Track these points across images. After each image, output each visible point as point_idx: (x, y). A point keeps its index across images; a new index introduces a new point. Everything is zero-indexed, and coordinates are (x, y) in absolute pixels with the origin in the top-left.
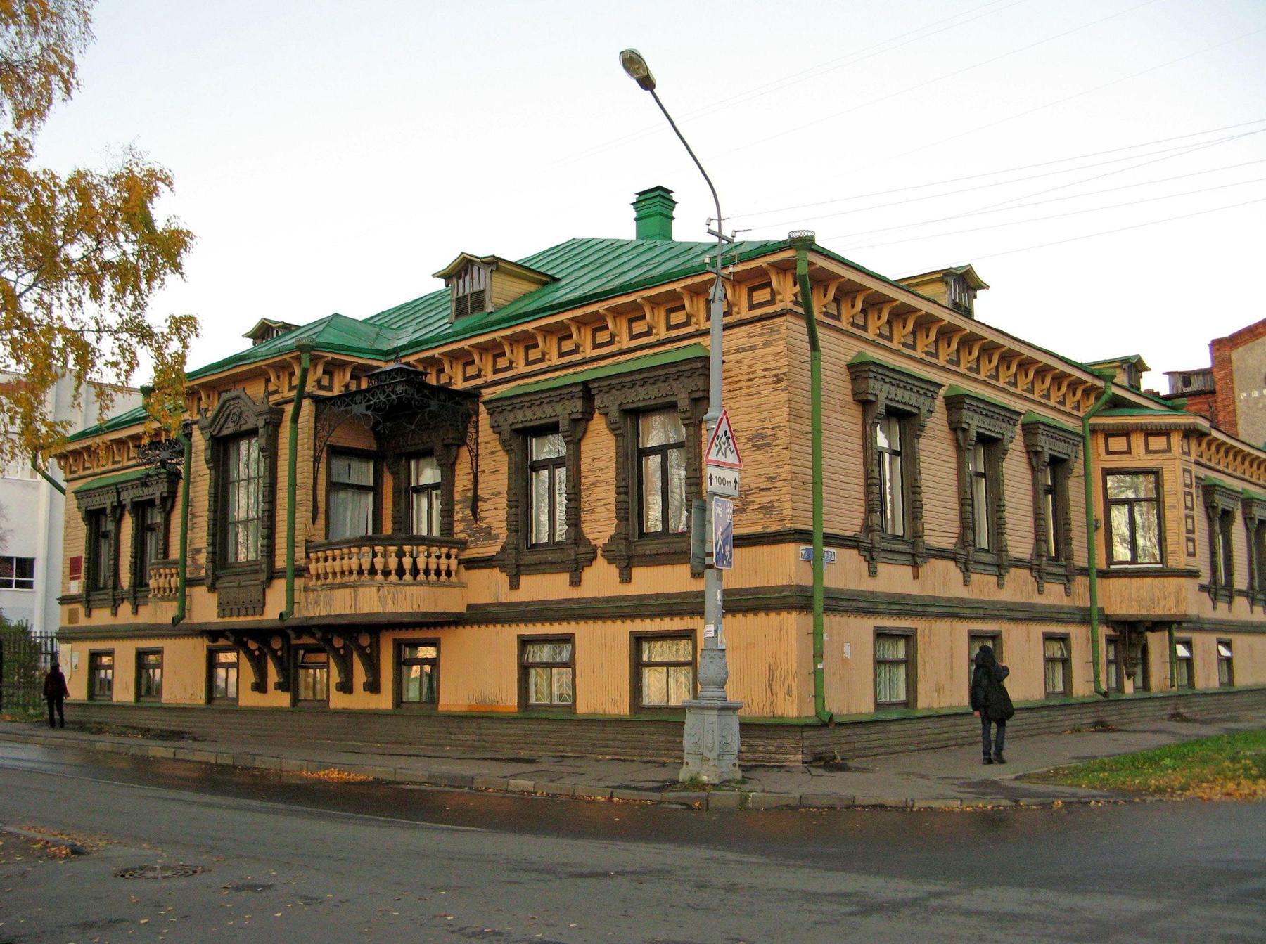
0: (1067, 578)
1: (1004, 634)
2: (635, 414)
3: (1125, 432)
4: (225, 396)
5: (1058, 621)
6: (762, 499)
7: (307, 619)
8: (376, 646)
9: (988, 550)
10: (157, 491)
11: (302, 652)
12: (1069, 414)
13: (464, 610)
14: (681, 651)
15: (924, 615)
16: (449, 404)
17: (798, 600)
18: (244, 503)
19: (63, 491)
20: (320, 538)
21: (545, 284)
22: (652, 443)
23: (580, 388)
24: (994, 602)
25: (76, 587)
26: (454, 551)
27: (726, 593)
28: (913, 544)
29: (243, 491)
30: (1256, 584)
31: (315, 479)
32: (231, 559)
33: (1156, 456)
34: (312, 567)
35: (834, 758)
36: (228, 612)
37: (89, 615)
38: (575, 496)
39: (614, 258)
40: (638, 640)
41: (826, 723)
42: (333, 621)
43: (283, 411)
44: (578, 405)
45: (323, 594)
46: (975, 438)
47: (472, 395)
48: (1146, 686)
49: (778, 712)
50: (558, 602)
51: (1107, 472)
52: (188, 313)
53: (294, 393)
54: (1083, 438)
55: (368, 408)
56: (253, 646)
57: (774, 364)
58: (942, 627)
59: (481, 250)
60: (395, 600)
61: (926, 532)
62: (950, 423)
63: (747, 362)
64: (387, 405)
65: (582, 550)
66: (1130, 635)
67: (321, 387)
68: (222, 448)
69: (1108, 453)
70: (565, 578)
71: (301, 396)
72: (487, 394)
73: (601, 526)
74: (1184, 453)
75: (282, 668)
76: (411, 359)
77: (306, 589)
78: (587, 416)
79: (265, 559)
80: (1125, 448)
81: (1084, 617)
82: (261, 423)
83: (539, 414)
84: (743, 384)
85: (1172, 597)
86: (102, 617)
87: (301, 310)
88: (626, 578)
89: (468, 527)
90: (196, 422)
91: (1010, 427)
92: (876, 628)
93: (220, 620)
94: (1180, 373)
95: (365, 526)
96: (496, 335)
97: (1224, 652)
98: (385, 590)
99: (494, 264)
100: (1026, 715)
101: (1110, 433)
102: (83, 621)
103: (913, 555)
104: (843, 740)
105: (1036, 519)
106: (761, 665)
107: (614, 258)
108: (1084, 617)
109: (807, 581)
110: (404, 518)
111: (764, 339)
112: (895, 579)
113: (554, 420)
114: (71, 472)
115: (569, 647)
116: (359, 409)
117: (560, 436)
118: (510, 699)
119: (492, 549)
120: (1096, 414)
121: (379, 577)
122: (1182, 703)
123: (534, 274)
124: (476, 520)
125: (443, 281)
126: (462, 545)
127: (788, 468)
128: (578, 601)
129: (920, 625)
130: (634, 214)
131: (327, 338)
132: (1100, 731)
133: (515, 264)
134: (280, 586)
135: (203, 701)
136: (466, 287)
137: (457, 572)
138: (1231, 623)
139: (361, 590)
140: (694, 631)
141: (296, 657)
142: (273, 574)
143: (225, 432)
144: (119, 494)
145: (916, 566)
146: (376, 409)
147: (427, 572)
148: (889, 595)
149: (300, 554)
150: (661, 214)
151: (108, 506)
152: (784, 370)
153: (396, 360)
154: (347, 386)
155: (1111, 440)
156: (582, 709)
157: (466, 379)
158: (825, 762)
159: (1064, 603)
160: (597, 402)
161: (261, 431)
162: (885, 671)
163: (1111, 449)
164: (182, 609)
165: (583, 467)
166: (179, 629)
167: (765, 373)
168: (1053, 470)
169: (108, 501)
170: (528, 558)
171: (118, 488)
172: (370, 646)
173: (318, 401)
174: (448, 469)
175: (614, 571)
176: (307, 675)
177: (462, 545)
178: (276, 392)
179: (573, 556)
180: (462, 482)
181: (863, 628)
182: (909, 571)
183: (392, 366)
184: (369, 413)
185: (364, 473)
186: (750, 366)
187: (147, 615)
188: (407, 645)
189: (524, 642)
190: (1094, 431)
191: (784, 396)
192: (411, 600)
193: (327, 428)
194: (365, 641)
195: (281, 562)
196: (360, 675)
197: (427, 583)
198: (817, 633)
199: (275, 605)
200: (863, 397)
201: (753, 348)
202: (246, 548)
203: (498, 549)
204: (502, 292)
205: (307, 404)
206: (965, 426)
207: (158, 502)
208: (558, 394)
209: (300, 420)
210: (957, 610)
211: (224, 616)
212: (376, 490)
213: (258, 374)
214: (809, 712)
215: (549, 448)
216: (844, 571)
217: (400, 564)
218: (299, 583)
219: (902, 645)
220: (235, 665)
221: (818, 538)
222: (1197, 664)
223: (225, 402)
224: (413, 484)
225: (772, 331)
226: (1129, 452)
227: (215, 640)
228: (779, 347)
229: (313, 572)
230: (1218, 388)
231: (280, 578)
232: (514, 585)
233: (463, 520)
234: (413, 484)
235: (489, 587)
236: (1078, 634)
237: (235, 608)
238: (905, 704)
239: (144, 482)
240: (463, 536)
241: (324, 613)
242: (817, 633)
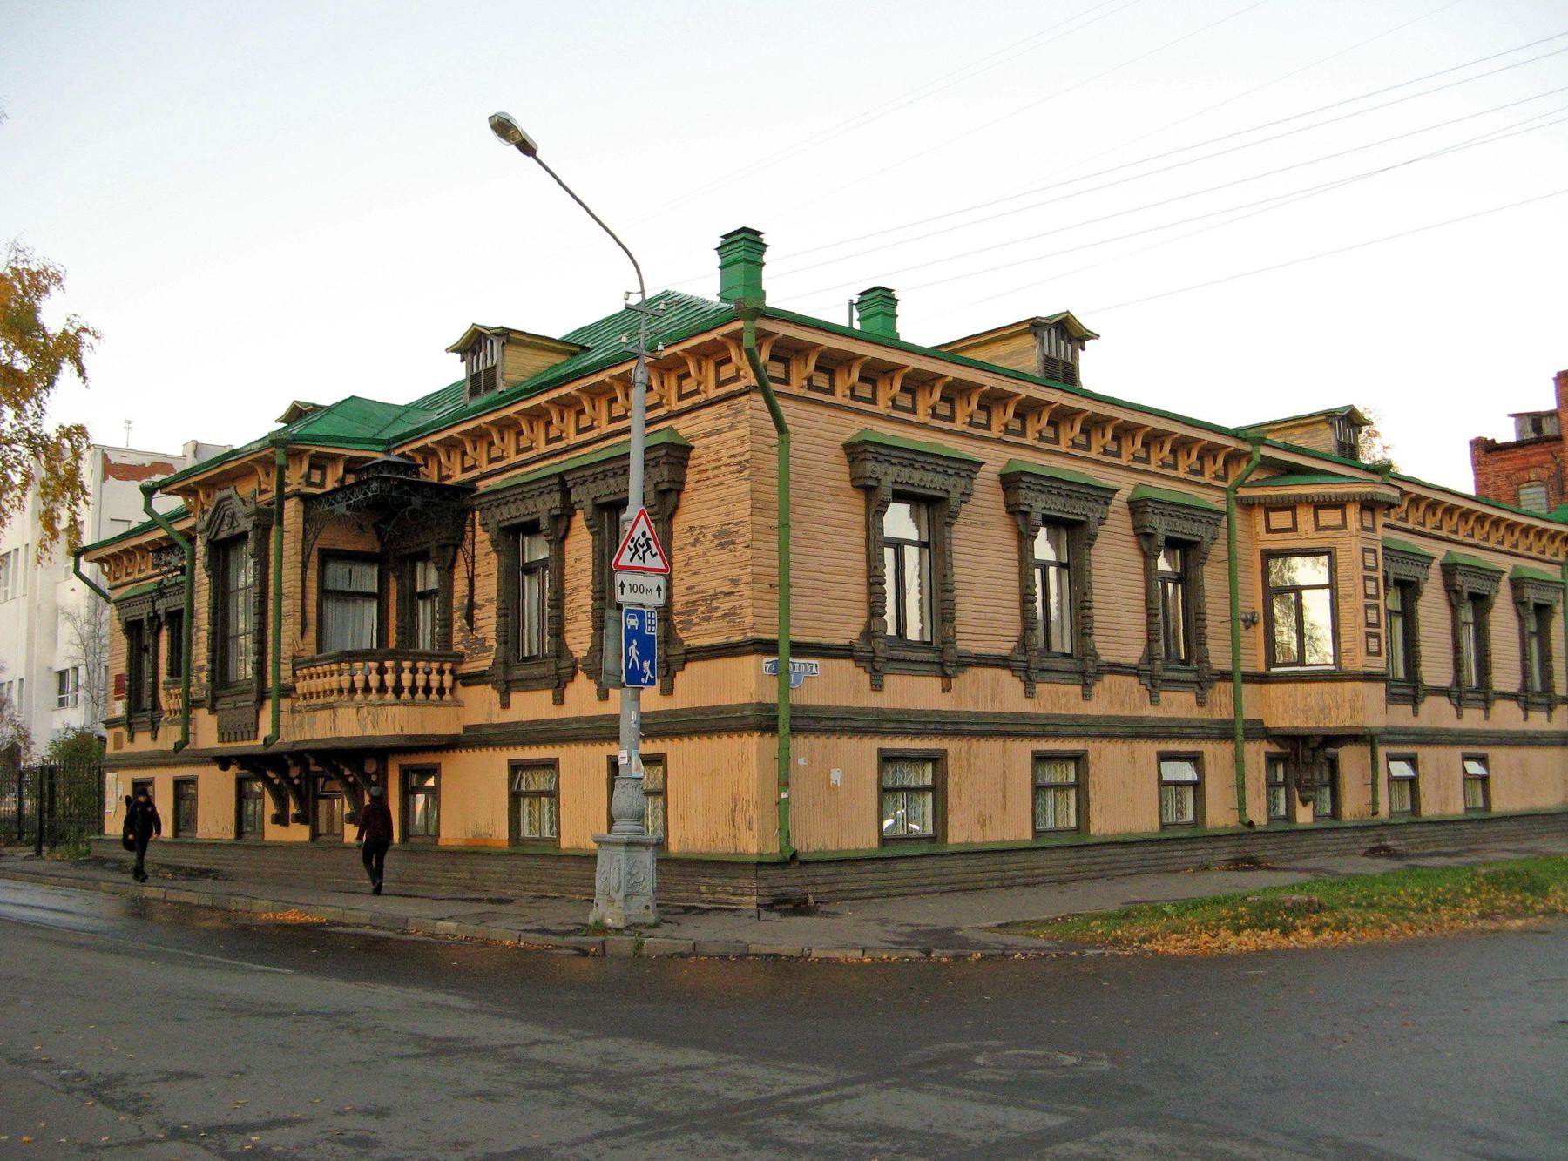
1: (1092, 756)
3: (1290, 505)
5: (1182, 737)
6: (725, 605)
7: (295, 743)
9: (1070, 655)
11: (321, 780)
12: (1209, 486)
13: (460, 731)
15: (955, 734)
17: (763, 721)
19: (107, 598)
20: (310, 650)
21: (574, 354)
23: (555, 481)
24: (1074, 717)
25: (119, 709)
26: (447, 666)
27: (643, 716)
28: (942, 651)
29: (241, 599)
32: (232, 678)
33: (1328, 533)
35: (806, 901)
37: (132, 740)
41: (792, 860)
42: (344, 745)
45: (307, 715)
47: (467, 488)
48: (1336, 813)
49: (741, 849)
50: (543, 722)
52: (79, 422)
54: (1227, 514)
55: (348, 507)
57: (739, 450)
58: (989, 749)
59: (492, 321)
60: (375, 722)
61: (959, 636)
62: (1008, 506)
63: (715, 448)
64: (377, 504)
65: (564, 663)
66: (1306, 756)
67: (309, 484)
68: (222, 552)
69: (1269, 530)
74: (1363, 528)
75: (301, 801)
76: (406, 449)
77: (293, 711)
80: (1289, 524)
81: (1224, 732)
82: (249, 526)
83: (523, 510)
84: (710, 474)
85: (1347, 705)
89: (465, 638)
91: (1100, 508)
92: (881, 751)
93: (220, 745)
94: (1529, 414)
95: (369, 641)
97: (1474, 768)
98: (364, 711)
99: (507, 336)
100: (1118, 851)
101: (1271, 506)
102: (128, 748)
103: (941, 664)
104: (819, 880)
105: (1148, 615)
106: (717, 798)
108: (1224, 732)
109: (771, 698)
110: (408, 631)
111: (729, 420)
112: (1058, 699)
114: (116, 579)
115: (660, 768)
116: (341, 509)
118: (502, 832)
119: (484, 663)
121: (359, 696)
122: (1397, 837)
124: (472, 630)
126: (459, 659)
127: (749, 569)
128: (560, 721)
129: (952, 746)
130: (718, 262)
132: (1245, 869)
135: (232, 837)
137: (452, 691)
138: (1488, 734)
139: (340, 711)
141: (316, 786)
143: (222, 535)
145: (945, 676)
147: (413, 690)
148: (901, 712)
149: (286, 671)
150: (746, 261)
151: (145, 617)
152: (747, 456)
153: (387, 452)
154: (342, 480)
155: (1321, 513)
158: (791, 905)
159: (1195, 715)
162: (889, 799)
163: (1273, 526)
164: (186, 733)
165: (567, 570)
167: (732, 460)
170: (517, 673)
172: (376, 772)
173: (306, 499)
174: (447, 572)
177: (459, 659)
180: (460, 587)
182: (936, 683)
183: (381, 457)
185: (368, 579)
186: (717, 452)
188: (415, 772)
190: (1248, 505)
191: (747, 486)
192: (394, 722)
194: (371, 767)
197: (412, 702)
198: (784, 759)
200: (862, 482)
201: (719, 431)
202: (244, 669)
203: (490, 662)
204: (516, 368)
206: (1024, 508)
210: (1010, 728)
212: (381, 597)
214: (773, 848)
215: (536, 550)
217: (382, 682)
218: (285, 704)
219: (929, 768)
221: (784, 648)
222: (1424, 786)
223: (219, 502)
224: (419, 589)
225: (738, 412)
226: (1294, 529)
228: (743, 430)
230: (1565, 432)
233: (461, 630)
234: (419, 589)
235: (481, 706)
236: (1216, 753)
238: (932, 839)
240: (459, 648)
241: (308, 737)
242: (784, 759)
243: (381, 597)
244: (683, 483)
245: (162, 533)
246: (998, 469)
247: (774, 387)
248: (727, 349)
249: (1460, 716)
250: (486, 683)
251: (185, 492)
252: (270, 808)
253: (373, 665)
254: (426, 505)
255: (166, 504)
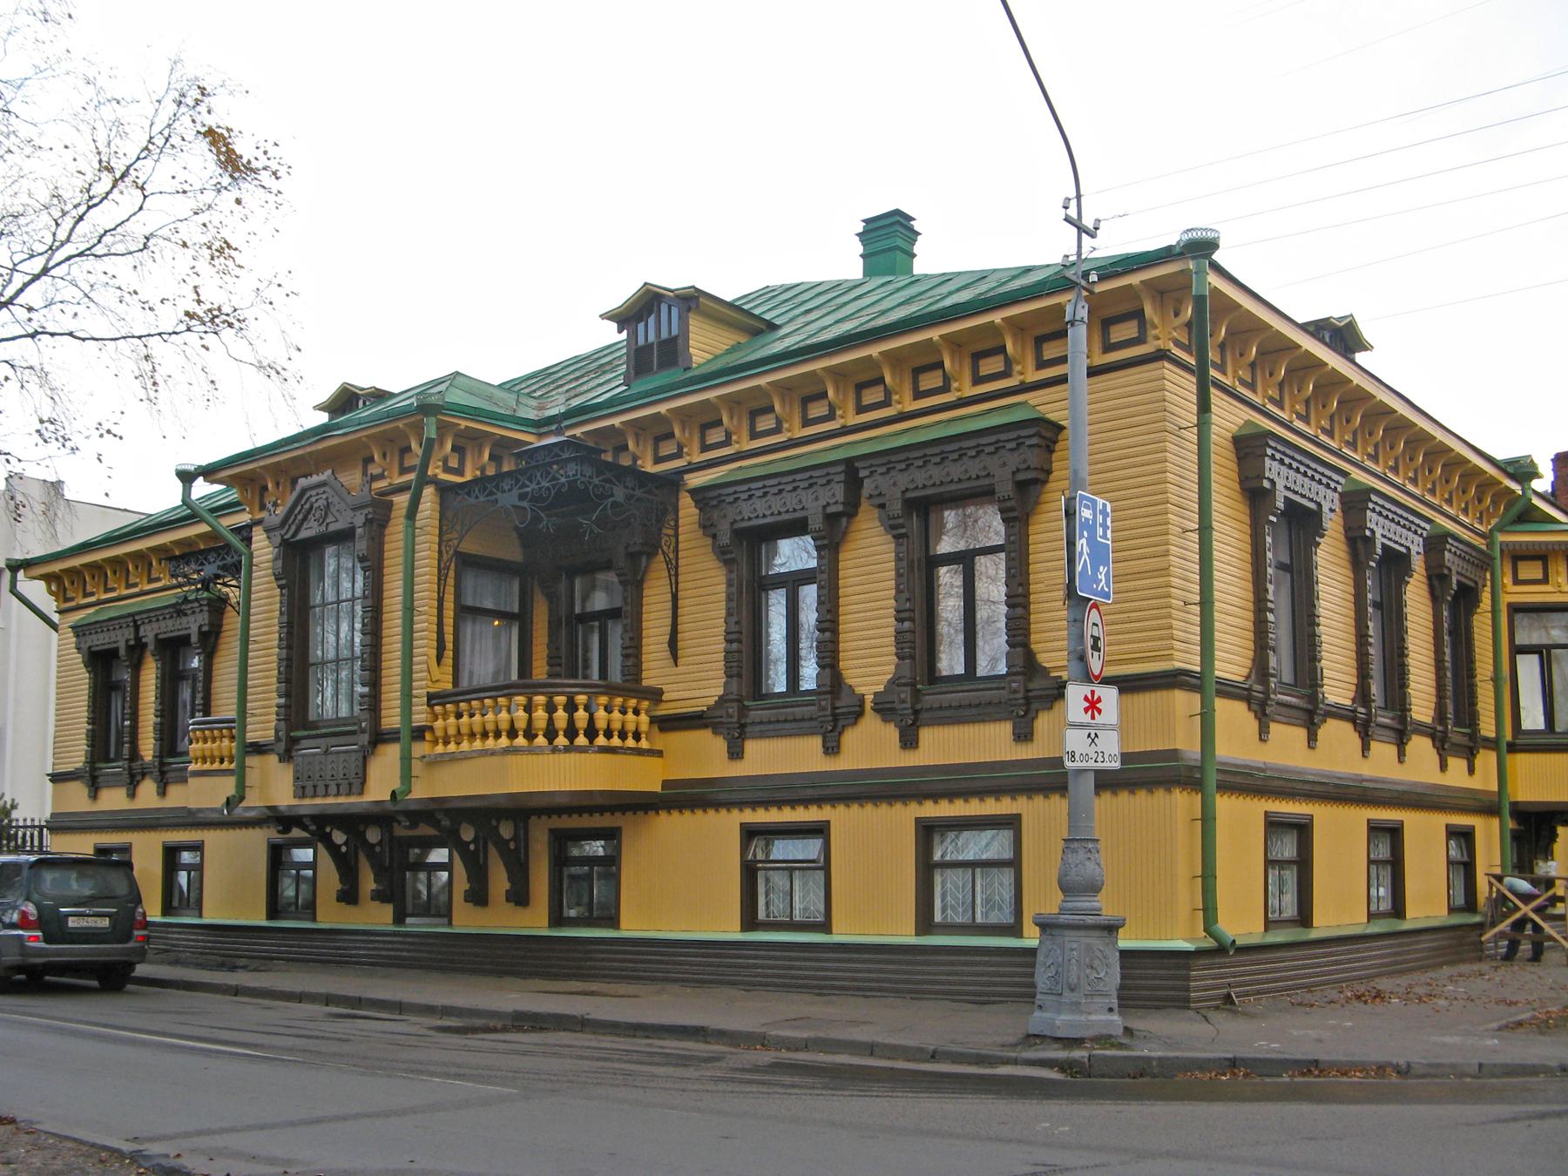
0: (1469, 754)
2: (921, 511)
4: (303, 482)
8: (522, 837)
10: (194, 624)
13: (659, 789)
14: (809, 849)
16: (638, 493)
18: (338, 635)
19: (54, 626)
22: (945, 546)
23: (840, 468)
30: (1375, 689)
31: (441, 601)
32: (312, 716)
34: (439, 724)
36: (309, 790)
38: (829, 623)
39: (856, 299)
40: (928, 831)
43: (390, 505)
44: (838, 491)
46: (1280, 505)
47: (672, 482)
51: (1515, 609)
53: (412, 476)
55: (522, 497)
56: (339, 837)
59: (672, 279)
67: (447, 470)
68: (298, 560)
69: (1516, 582)
70: (1005, 729)
71: (424, 480)
72: (696, 480)
73: (871, 666)
75: (380, 872)
78: (851, 508)
79: (366, 715)
80: (1540, 576)
81: (1487, 806)
82: (359, 519)
86: (113, 799)
87: (399, 371)
88: (909, 741)
90: (259, 522)
92: (551, 831)
96: (662, 409)
99: (692, 300)
107: (856, 299)
108: (1487, 806)
113: (798, 515)
114: (67, 600)
116: (508, 499)
117: (808, 538)
120: (1501, 528)
123: (745, 319)
125: (614, 326)
130: (860, 249)
131: (456, 397)
133: (730, 305)
134: (390, 754)
136: (649, 333)
140: (1019, 816)
142: (380, 738)
143: (304, 534)
144: (137, 628)
146: (535, 499)
156: (841, 934)
157: (658, 460)
160: (868, 487)
161: (359, 531)
163: (1521, 577)
166: (229, 819)
168: (1456, 604)
169: (121, 639)
171: (134, 621)
173: (444, 490)
174: (634, 585)
175: (891, 733)
176: (416, 880)
178: (381, 477)
179: (833, 712)
181: (1256, 809)
184: (524, 504)
187: (178, 797)
189: (750, 833)
193: (458, 527)
195: (391, 718)
196: (499, 881)
199: (382, 780)
202: (332, 699)
205: (429, 492)
207: (194, 639)
208: (811, 475)
209: (419, 516)
211: (303, 796)
212: (522, 619)
213: (336, 459)
215: (794, 554)
216: (1235, 736)
217: (571, 722)
218: (420, 749)
220: (312, 865)
223: (304, 491)
224: (577, 610)
227: (287, 830)
229: (439, 733)
231: (386, 741)
232: (736, 753)
234: (577, 610)
237: (321, 785)
239: (178, 610)
243: (522, 619)
244: (1049, 472)
245: (203, 528)
246: (1234, 428)
247: (1213, 373)
248: (407, 438)
249: (1443, 767)
250: (705, 726)
251: (230, 482)
252: (329, 878)
253: (540, 699)
254: (629, 498)
255: (201, 488)
